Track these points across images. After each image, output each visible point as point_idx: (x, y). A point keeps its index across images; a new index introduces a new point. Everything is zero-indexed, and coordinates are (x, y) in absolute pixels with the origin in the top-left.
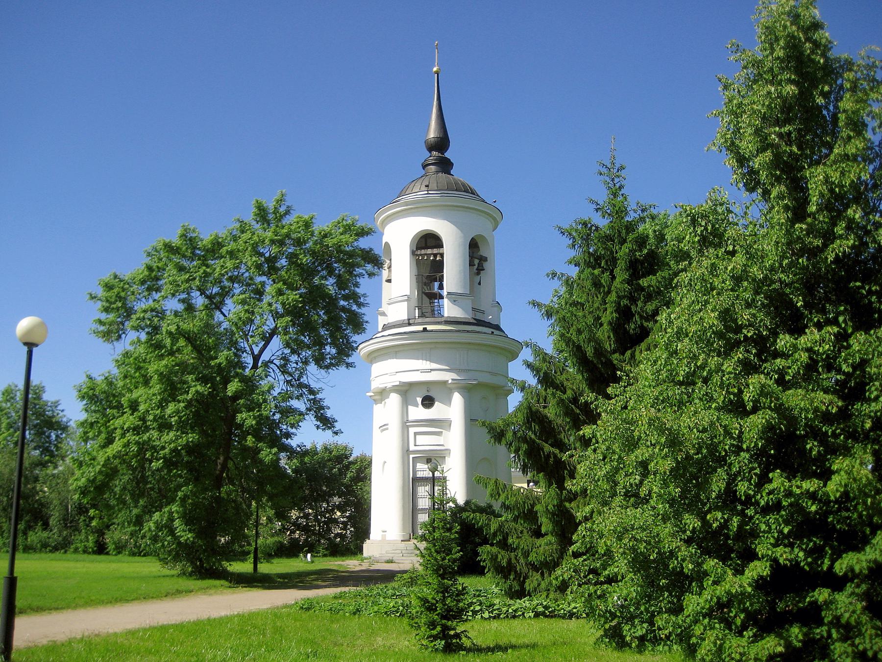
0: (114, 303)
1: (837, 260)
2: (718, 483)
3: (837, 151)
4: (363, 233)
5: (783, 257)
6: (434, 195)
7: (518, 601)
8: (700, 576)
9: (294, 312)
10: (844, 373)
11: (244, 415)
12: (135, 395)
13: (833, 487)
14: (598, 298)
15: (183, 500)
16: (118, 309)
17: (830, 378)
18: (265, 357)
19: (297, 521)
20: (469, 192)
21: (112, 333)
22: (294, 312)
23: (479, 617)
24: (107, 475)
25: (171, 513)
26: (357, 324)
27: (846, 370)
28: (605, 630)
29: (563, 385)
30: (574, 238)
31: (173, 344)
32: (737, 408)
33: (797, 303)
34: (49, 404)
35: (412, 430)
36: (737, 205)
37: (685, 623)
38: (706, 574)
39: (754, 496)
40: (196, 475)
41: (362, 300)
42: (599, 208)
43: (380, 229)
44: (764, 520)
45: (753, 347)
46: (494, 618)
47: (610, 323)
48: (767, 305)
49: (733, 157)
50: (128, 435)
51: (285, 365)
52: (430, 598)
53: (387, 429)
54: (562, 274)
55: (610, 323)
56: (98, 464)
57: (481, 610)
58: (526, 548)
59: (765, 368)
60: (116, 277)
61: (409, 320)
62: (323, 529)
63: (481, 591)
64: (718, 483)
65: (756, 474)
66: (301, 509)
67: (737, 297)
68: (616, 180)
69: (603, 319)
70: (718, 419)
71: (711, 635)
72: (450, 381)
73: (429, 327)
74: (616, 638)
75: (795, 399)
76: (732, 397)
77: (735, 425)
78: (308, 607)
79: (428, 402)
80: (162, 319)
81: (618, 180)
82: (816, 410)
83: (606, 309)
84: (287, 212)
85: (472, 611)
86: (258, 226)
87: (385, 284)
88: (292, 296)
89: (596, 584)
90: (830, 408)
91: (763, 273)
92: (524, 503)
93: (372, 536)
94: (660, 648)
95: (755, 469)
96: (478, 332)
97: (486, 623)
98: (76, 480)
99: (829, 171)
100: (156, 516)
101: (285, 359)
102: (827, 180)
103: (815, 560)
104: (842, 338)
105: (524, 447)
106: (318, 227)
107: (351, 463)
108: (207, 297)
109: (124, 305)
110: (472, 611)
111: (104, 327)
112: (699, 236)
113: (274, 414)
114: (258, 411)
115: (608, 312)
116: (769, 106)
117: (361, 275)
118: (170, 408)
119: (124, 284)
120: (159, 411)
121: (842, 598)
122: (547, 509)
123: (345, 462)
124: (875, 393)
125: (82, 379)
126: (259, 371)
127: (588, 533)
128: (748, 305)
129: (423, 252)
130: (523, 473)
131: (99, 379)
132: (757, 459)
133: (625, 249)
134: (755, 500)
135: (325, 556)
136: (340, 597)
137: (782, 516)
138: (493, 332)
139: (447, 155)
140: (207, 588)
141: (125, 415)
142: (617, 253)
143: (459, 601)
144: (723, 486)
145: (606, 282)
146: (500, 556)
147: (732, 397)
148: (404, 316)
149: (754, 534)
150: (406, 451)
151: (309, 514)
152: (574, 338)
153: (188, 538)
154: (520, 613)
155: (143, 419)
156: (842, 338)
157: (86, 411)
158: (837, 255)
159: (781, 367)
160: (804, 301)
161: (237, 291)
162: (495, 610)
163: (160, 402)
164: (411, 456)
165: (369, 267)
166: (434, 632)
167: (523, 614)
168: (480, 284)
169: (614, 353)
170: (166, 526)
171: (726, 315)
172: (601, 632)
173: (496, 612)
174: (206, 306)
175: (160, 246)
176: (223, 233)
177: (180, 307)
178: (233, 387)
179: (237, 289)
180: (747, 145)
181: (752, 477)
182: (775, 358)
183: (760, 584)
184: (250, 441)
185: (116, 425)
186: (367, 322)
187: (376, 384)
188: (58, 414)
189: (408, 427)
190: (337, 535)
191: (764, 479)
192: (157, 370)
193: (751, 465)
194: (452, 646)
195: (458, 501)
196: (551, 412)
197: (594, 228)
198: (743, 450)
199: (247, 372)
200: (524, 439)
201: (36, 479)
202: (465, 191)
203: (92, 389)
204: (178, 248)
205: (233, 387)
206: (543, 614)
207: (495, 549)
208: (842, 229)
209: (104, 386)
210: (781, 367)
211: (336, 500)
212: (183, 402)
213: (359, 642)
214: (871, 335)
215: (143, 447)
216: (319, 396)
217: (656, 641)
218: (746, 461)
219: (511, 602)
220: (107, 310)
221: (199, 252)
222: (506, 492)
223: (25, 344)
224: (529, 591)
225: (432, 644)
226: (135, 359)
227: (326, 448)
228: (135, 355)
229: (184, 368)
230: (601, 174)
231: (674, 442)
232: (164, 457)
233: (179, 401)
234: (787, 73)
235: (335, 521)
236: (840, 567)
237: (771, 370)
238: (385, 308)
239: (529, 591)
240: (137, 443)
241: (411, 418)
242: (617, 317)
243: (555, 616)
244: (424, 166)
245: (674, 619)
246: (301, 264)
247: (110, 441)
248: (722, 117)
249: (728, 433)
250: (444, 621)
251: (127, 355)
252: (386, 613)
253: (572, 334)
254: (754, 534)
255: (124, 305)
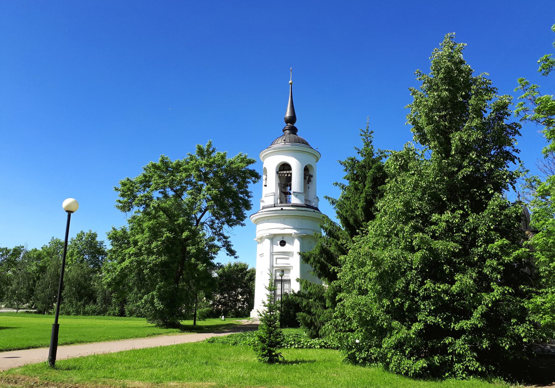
0: (127, 192)
1: (464, 177)
2: (400, 284)
3: (467, 125)
4: (250, 162)
5: (436, 176)
6: (288, 145)
7: (313, 340)
8: (391, 329)
9: (215, 198)
10: (465, 233)
11: (191, 248)
12: (137, 237)
13: (455, 288)
14: (357, 195)
15: (159, 289)
16: (128, 195)
17: (458, 236)
18: (202, 220)
19: (220, 300)
20: (305, 144)
21: (126, 207)
22: (215, 198)
23: (293, 347)
24: (122, 277)
25: (153, 296)
26: (248, 206)
27: (466, 232)
28: (348, 355)
29: (338, 236)
30: (347, 166)
31: (156, 213)
32: (412, 250)
33: (444, 198)
34: (99, 242)
35: (275, 257)
36: (420, 151)
37: (385, 352)
38: (393, 329)
39: (418, 291)
40: (165, 277)
41: (250, 194)
42: (360, 152)
43: (262, 161)
44: (423, 303)
45: (420, 219)
46: (300, 348)
47: (362, 207)
48: (430, 199)
49: (414, 128)
50: (132, 257)
51: (212, 225)
52: (263, 336)
53: (263, 256)
54: (341, 184)
55: (362, 207)
56: (118, 271)
57: (294, 344)
58: (320, 314)
59: (426, 230)
60: (128, 180)
61: (274, 204)
62: (233, 304)
63: (298, 335)
64: (400, 284)
65: (419, 281)
66: (222, 294)
67: (414, 196)
68: (369, 138)
69: (358, 205)
70: (402, 253)
71: (395, 358)
72: (293, 234)
73: (284, 208)
74: (352, 359)
75: (439, 245)
76: (408, 243)
77: (410, 257)
78: (212, 341)
79: (283, 243)
80: (151, 201)
81: (370, 138)
82: (449, 251)
83: (360, 201)
84: (213, 151)
85: (290, 344)
86: (199, 158)
87: (264, 187)
88: (215, 191)
89: (344, 332)
90: (455, 250)
91: (426, 184)
92: (319, 292)
93: (255, 307)
94: (373, 364)
95: (419, 278)
96: (307, 211)
97: (296, 350)
98: (106, 279)
99: (463, 135)
100: (146, 297)
101: (213, 222)
102: (461, 139)
103: (447, 323)
104: (464, 216)
105: (319, 265)
106: (228, 159)
107: (248, 272)
108: (174, 191)
109: (132, 193)
110: (290, 344)
111: (122, 204)
112: (399, 166)
113: (205, 248)
114: (197, 246)
115: (361, 202)
116: (434, 102)
117: (249, 182)
118: (153, 244)
119: (132, 183)
120: (148, 246)
121: (459, 342)
122: (329, 295)
123: (245, 272)
124: (480, 243)
125: (110, 230)
126: (199, 227)
127: (342, 307)
128: (420, 199)
129: (282, 172)
130: (319, 278)
131: (119, 230)
132: (421, 273)
133: (371, 172)
134: (418, 293)
135: (232, 317)
136: (231, 337)
137: (431, 302)
138: (314, 211)
139: (295, 125)
140: (169, 332)
141: (131, 248)
142: (367, 174)
143: (277, 338)
144: (402, 285)
145: (361, 188)
146: (307, 318)
147: (408, 243)
148: (272, 203)
149: (418, 310)
150: (272, 267)
151: (226, 297)
152: (344, 214)
153: (161, 307)
154: (313, 346)
155: (140, 249)
156: (464, 216)
157: (112, 245)
158: (463, 175)
159: (433, 229)
160: (447, 198)
161: (189, 189)
162: (301, 344)
163: (149, 242)
164: (274, 269)
165: (253, 178)
166: (264, 353)
167: (315, 346)
168: (309, 188)
169: (363, 222)
170: (150, 301)
171: (407, 204)
172: (347, 356)
173: (302, 345)
174: (174, 195)
175: (150, 165)
176: (182, 161)
177: (161, 196)
178: (185, 234)
179: (189, 188)
180: (423, 121)
181: (417, 282)
182: (431, 225)
183: (419, 334)
184: (193, 260)
185: (126, 252)
186: (252, 205)
187: (259, 235)
188: (103, 247)
189: (273, 255)
190: (239, 307)
191: (422, 283)
192: (148, 226)
193: (417, 277)
194: (272, 359)
195: (295, 291)
196: (332, 249)
197: (356, 162)
198: (413, 269)
199: (193, 228)
200: (319, 262)
201: (91, 279)
202: (303, 143)
203: (115, 234)
204: (159, 167)
205: (185, 234)
206: (324, 346)
207: (304, 314)
208: (467, 163)
209: (121, 233)
210: (433, 229)
211: (240, 290)
212: (160, 241)
213: (232, 358)
214: (480, 215)
215: (139, 263)
216: (228, 240)
217: (371, 361)
218: (414, 274)
219: (309, 340)
220: (122, 195)
221: (170, 169)
222: (311, 287)
223: (67, 211)
224: (320, 335)
225: (263, 359)
226: (138, 220)
227: (235, 265)
228: (138, 218)
229: (163, 225)
230: (361, 135)
231: (378, 263)
232: (150, 268)
233: (158, 241)
234: (445, 86)
235: (239, 301)
236: (457, 327)
237: (429, 231)
238: (263, 198)
239: (320, 335)
240: (137, 261)
241: (275, 251)
242: (365, 205)
243: (329, 348)
244: (284, 131)
245: (379, 350)
246: (220, 176)
247: (123, 260)
248: (412, 108)
249: (406, 261)
250: (269, 348)
251: (134, 218)
252: (249, 344)
253: (343, 212)
254: (418, 310)
255: (132, 193)
